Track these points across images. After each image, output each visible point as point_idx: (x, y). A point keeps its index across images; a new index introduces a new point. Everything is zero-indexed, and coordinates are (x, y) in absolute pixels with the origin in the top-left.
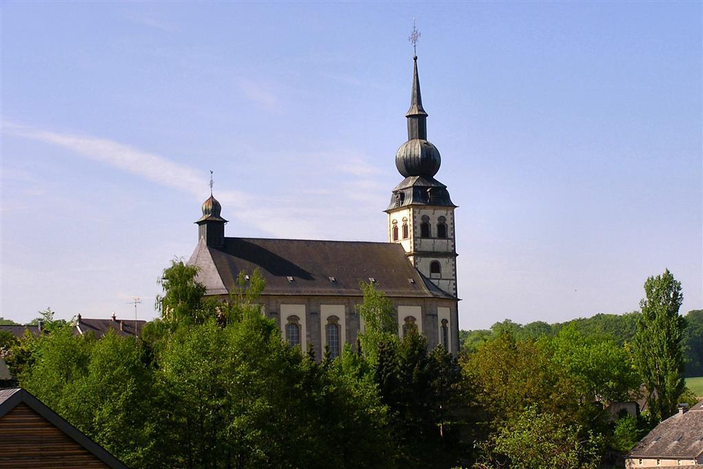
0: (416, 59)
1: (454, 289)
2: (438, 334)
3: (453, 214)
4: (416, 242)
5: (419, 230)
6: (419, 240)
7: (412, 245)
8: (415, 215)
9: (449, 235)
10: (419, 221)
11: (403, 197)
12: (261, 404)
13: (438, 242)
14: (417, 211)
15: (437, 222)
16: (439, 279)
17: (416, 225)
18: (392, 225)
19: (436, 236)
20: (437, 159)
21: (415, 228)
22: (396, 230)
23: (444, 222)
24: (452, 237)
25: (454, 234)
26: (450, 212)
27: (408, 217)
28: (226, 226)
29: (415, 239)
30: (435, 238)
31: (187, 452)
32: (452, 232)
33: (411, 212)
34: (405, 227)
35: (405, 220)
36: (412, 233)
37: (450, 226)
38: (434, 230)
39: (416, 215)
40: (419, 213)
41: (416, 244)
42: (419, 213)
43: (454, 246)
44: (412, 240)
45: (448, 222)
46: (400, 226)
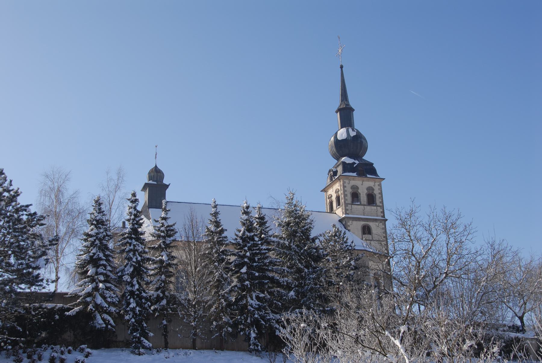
0: (342, 67)
1: (381, 212)
2: (352, 214)
3: (380, 185)
4: (347, 208)
5: (349, 198)
6: (350, 206)
7: (344, 210)
8: (345, 185)
9: (378, 201)
10: (349, 190)
11: (335, 173)
12: (304, 311)
13: (368, 208)
14: (347, 181)
15: (366, 191)
16: (371, 240)
17: (346, 193)
18: (328, 200)
19: (365, 203)
20: (366, 162)
21: (345, 195)
22: (331, 203)
23: (373, 192)
24: (381, 205)
25: (382, 202)
26: (377, 184)
27: (339, 188)
28: (168, 192)
29: (346, 205)
30: (364, 205)
31: (240, 319)
32: (380, 200)
33: (342, 183)
34: (338, 198)
35: (337, 192)
36: (343, 201)
37: (378, 196)
38: (364, 198)
39: (346, 185)
40: (349, 184)
41: (348, 210)
42: (349, 184)
43: (383, 212)
44: (343, 206)
45: (376, 192)
46: (334, 198)
